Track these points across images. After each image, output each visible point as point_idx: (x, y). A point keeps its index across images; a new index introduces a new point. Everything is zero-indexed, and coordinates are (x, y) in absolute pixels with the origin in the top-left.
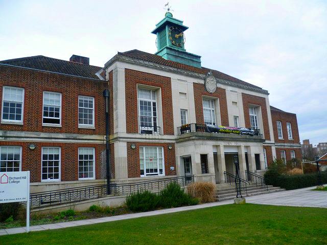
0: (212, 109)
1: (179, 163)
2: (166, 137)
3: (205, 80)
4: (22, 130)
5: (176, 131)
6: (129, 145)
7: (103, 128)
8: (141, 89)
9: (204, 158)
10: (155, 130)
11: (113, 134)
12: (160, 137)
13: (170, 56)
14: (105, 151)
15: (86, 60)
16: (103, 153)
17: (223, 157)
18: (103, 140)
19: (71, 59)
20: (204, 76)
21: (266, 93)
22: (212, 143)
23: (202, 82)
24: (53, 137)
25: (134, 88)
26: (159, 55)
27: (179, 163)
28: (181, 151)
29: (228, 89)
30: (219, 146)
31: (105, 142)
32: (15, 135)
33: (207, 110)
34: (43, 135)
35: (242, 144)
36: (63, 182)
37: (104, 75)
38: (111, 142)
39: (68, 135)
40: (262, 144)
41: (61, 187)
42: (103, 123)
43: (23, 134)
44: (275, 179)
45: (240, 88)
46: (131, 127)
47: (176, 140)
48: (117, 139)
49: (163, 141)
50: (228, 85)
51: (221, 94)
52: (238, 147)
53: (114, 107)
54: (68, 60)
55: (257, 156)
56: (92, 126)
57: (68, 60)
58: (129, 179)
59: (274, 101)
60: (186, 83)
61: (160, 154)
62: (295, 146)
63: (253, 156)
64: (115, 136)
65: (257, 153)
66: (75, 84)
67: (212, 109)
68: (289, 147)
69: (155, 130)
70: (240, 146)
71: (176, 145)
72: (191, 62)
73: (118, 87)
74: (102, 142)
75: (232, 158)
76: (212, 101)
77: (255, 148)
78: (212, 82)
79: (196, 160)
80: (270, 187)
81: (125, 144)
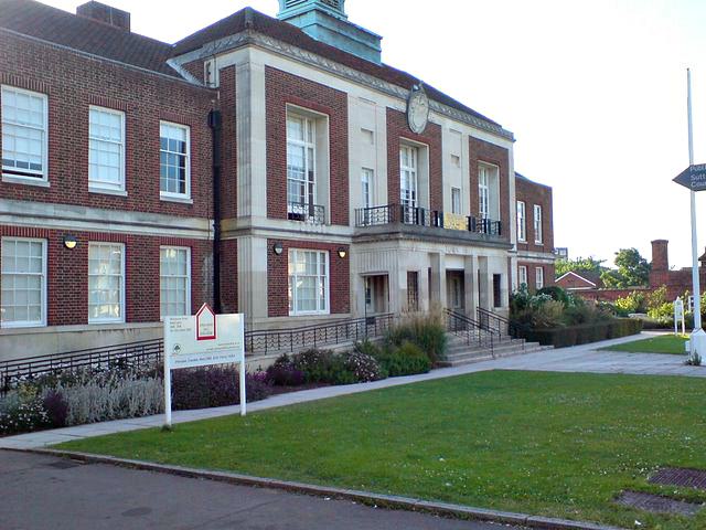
0: (307, 145)
1: (357, 288)
2: (335, 229)
3: (408, 102)
4: (49, 200)
5: (352, 221)
6: (273, 244)
7: (208, 202)
8: (294, 111)
9: (413, 277)
10: (311, 214)
11: (234, 216)
12: (319, 229)
13: (322, 32)
14: (212, 258)
15: (122, 18)
16: (208, 261)
17: (443, 276)
18: (209, 231)
19: (81, 9)
20: (406, 92)
21: (509, 137)
22: (426, 247)
23: (402, 107)
24: (111, 219)
25: (282, 114)
26: (293, 22)
27: (357, 288)
28: (361, 263)
29: (447, 125)
30: (438, 254)
31: (212, 235)
32: (33, 213)
33: (295, 145)
34: (91, 213)
35: (475, 252)
36: (51, 329)
37: (197, 68)
38: (226, 237)
39: (141, 215)
40: (506, 252)
41: (128, 338)
42: (208, 190)
43: (50, 210)
44: (527, 325)
45: (468, 123)
46: (276, 208)
47: (353, 237)
48: (247, 231)
49: (329, 240)
50: (446, 115)
51: (433, 135)
52: (465, 257)
53: (239, 154)
54: (74, 12)
55: (497, 278)
56: (186, 197)
57: (74, 12)
58: (272, 319)
59: (526, 163)
60: (373, 108)
61: (323, 261)
62: (546, 259)
63: (491, 278)
64: (241, 224)
65: (497, 273)
66: (152, 91)
67: (307, 145)
68: (535, 261)
69: (311, 214)
70: (471, 257)
71: (353, 249)
72: (362, 48)
73: (252, 110)
74: (207, 234)
75: (457, 278)
76: (310, 123)
77: (494, 261)
78: (421, 109)
79: (400, 283)
80: (518, 343)
81: (264, 244)
